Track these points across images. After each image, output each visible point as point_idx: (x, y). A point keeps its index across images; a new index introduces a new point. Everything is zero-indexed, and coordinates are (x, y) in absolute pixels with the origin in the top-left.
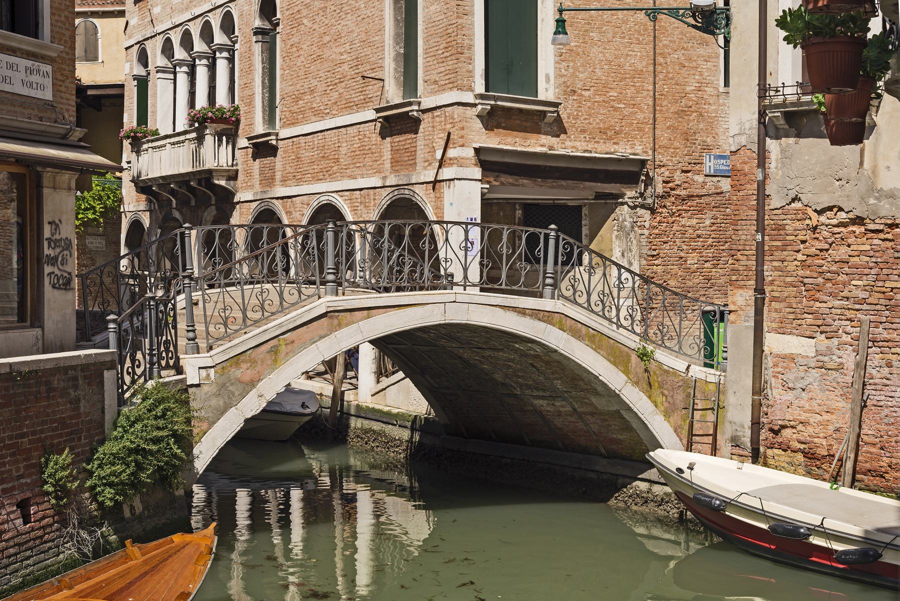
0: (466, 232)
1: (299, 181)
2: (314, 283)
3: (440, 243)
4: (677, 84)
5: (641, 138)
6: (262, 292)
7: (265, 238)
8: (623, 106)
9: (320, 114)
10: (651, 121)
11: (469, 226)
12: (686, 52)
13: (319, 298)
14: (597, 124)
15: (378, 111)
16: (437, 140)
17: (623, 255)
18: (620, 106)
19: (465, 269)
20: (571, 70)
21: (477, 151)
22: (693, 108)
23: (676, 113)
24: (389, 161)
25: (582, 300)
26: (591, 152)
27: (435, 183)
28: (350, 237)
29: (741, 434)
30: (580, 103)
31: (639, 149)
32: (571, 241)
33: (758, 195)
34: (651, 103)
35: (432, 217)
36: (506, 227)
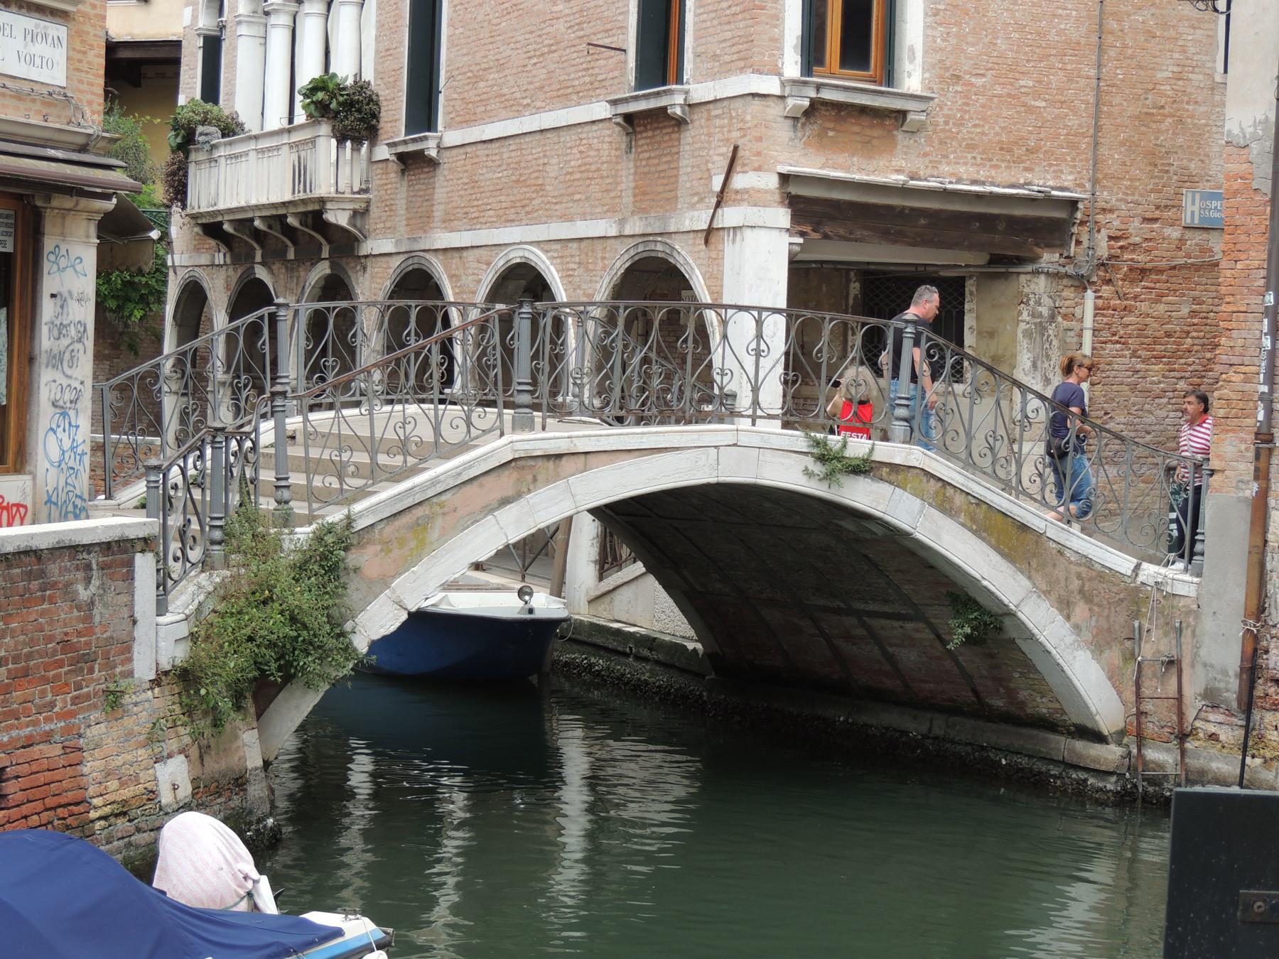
0: (759, 323)
1: (474, 223)
2: (492, 404)
3: (715, 339)
4: (1140, 67)
5: (1073, 160)
6: (404, 423)
7: (413, 325)
8: (1044, 104)
9: (516, 108)
10: (1091, 131)
11: (765, 314)
12: (1157, 12)
13: (502, 434)
14: (997, 134)
15: (614, 103)
16: (716, 158)
17: (1034, 365)
18: (1037, 104)
19: (755, 390)
20: (953, 41)
21: (785, 178)
22: (1167, 110)
23: (1137, 117)
24: (630, 192)
25: (959, 446)
26: (983, 183)
27: (709, 234)
28: (558, 325)
29: (1222, 685)
30: (967, 97)
31: (1068, 179)
32: (941, 341)
33: (1268, 269)
34: (1092, 100)
35: (705, 297)
36: (828, 317)
